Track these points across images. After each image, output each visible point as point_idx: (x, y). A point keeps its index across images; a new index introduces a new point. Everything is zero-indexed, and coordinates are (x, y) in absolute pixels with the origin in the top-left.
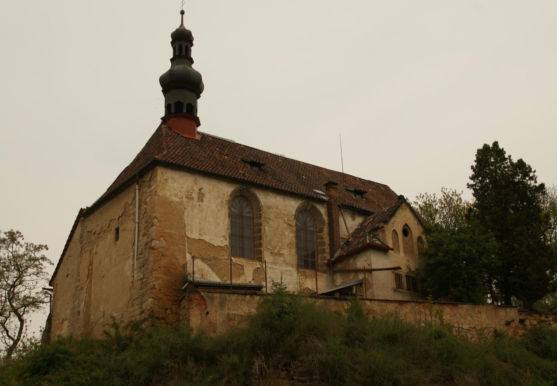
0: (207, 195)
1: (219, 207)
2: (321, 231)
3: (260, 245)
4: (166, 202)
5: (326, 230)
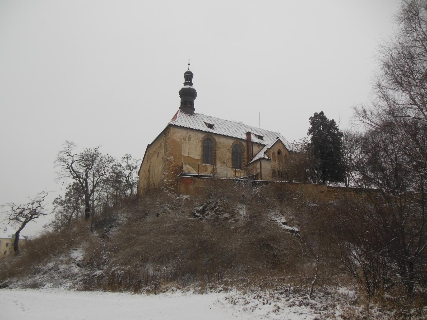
0: (192, 138)
1: (197, 143)
2: (244, 153)
3: (215, 159)
4: (174, 141)
5: (246, 152)
